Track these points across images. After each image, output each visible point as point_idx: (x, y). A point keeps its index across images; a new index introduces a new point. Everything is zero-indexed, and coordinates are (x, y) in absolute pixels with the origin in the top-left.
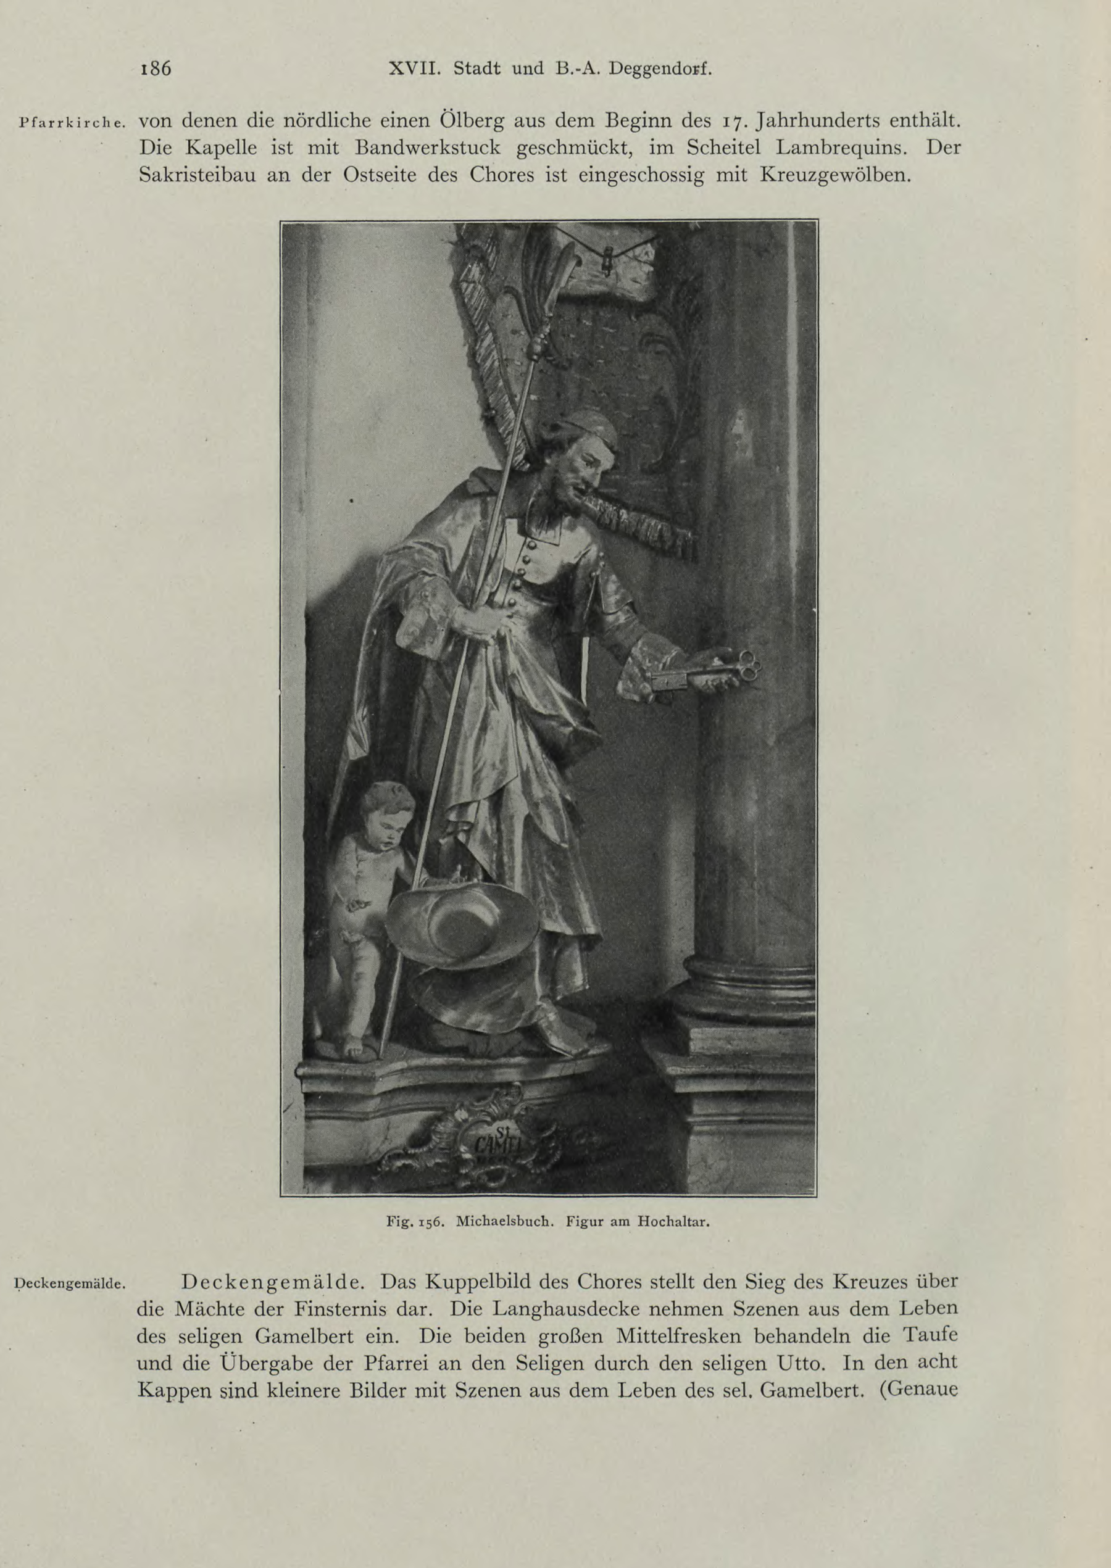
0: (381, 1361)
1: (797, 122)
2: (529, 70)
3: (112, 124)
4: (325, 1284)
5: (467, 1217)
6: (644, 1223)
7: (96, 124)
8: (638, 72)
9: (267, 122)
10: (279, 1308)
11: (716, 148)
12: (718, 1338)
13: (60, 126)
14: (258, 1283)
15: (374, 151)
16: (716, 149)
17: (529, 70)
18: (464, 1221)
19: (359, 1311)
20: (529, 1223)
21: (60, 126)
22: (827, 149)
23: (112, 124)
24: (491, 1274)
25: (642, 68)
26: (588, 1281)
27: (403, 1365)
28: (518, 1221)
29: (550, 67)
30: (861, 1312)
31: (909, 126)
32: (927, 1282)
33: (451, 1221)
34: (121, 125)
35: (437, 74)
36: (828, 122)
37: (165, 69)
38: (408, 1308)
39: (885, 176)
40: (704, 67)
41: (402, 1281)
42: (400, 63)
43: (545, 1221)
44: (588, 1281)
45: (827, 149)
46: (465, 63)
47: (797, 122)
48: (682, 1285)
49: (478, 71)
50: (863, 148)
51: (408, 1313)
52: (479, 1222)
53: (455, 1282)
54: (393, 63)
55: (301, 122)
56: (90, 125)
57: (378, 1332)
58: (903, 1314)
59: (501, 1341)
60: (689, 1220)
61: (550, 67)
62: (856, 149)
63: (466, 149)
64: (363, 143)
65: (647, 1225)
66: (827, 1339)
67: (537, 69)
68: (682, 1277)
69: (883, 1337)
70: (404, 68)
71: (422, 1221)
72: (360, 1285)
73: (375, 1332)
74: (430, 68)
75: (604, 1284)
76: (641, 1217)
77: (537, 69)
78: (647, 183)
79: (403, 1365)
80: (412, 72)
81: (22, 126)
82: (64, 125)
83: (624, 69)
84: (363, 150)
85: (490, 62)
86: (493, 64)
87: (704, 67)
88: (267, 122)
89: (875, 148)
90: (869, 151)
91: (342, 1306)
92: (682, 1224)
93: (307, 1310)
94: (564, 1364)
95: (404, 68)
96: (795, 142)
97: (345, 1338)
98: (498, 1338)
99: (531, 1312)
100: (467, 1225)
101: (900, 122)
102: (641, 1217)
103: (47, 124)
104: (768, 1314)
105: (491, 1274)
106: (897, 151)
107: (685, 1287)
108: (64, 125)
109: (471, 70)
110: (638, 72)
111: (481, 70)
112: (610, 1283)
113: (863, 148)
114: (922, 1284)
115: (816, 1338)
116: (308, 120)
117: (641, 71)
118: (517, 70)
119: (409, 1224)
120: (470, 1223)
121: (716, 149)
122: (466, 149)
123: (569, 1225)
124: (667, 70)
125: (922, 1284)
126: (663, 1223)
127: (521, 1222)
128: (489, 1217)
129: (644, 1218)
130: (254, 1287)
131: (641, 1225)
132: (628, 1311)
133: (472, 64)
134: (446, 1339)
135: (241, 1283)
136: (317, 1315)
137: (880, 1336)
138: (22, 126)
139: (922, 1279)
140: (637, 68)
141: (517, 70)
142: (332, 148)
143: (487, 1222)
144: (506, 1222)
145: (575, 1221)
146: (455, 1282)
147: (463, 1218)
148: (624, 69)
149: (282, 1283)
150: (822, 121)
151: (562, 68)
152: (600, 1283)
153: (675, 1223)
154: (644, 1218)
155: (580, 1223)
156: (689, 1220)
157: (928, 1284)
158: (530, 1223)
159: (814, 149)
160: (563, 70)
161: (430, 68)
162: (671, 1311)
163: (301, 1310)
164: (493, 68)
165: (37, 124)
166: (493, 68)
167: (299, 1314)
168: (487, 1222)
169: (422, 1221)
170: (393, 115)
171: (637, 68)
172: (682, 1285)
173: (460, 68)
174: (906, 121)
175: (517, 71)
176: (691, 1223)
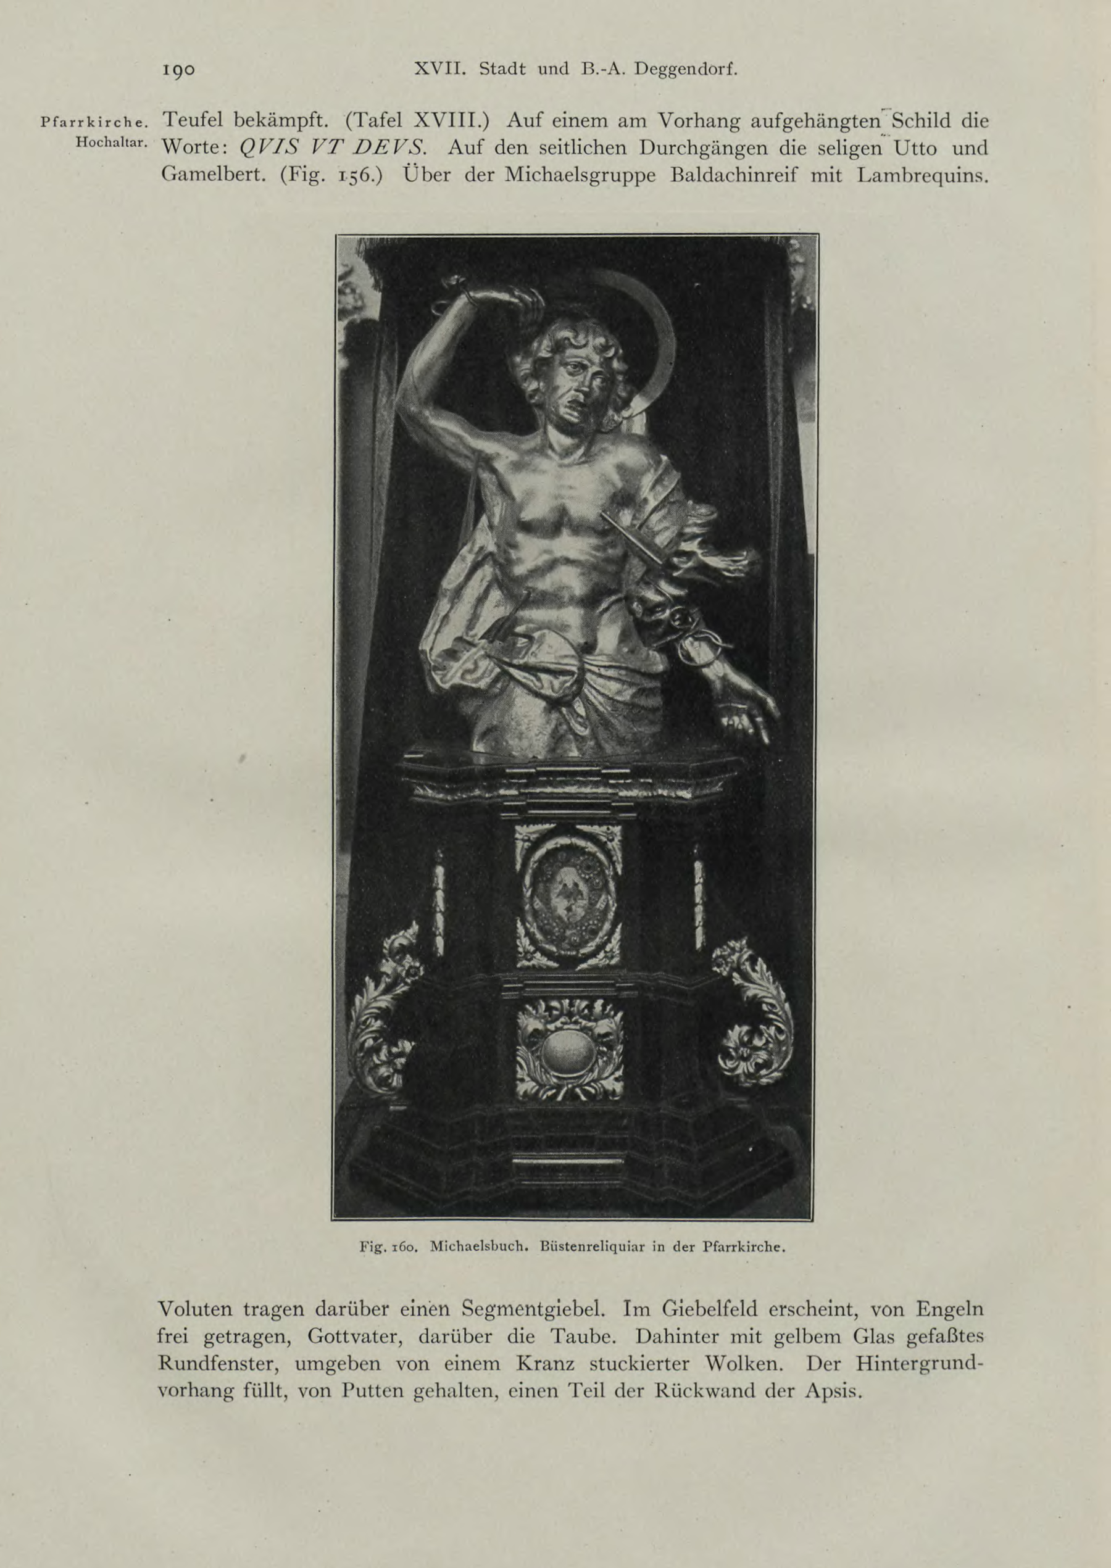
0: (55, 121)
1: (692, 123)
2: (555, 70)
3: (134, 124)
5: (441, 1243)
6: (82, 144)
7: (118, 124)
8: (668, 72)
10: (790, 1389)
13: (80, 126)
16: (599, 150)
17: (555, 70)
18: (438, 1246)
20: (503, 1248)
21: (80, 126)
22: (908, 177)
23: (134, 124)
25: (667, 69)
27: (731, 1249)
28: (492, 1246)
29: (576, 68)
33: (424, 1246)
35: (462, 75)
36: (970, 150)
37: (190, 70)
38: (430, 1335)
40: (729, 67)
41: (657, 1336)
42: (425, 63)
45: (908, 177)
46: (491, 64)
50: (944, 176)
51: (430, 1340)
52: (453, 1248)
53: (622, 175)
54: (418, 63)
56: (111, 124)
57: (456, 1359)
61: (576, 68)
62: (937, 177)
65: (85, 145)
67: (563, 70)
70: (429, 68)
73: (454, 1359)
74: (454, 68)
76: (79, 138)
77: (563, 70)
78: (593, 156)
79: (731, 1249)
80: (437, 72)
85: (515, 63)
86: (518, 65)
87: (729, 67)
89: (956, 176)
90: (950, 178)
91: (379, 1333)
94: (339, 1364)
96: (754, 116)
100: (441, 1250)
101: (869, 124)
102: (79, 138)
103: (68, 124)
106: (979, 179)
109: (496, 70)
110: (668, 72)
111: (506, 70)
113: (944, 176)
117: (667, 72)
118: (542, 70)
119: (382, 1249)
120: (444, 1248)
121: (599, 150)
123: (362, 1250)
124: (691, 70)
126: (574, 1248)
127: (495, 1247)
129: (82, 139)
131: (79, 145)
133: (129, 140)
140: (663, 69)
141: (542, 70)
142: (835, 176)
144: (480, 1248)
145: (369, 1248)
146: (622, 175)
147: (437, 1243)
151: (588, 68)
154: (82, 139)
155: (374, 1249)
158: (504, 1247)
159: (896, 177)
160: (589, 71)
161: (454, 68)
163: (295, 175)
164: (517, 69)
165: (58, 123)
166: (517, 69)
171: (663, 69)
173: (488, 68)
175: (543, 71)
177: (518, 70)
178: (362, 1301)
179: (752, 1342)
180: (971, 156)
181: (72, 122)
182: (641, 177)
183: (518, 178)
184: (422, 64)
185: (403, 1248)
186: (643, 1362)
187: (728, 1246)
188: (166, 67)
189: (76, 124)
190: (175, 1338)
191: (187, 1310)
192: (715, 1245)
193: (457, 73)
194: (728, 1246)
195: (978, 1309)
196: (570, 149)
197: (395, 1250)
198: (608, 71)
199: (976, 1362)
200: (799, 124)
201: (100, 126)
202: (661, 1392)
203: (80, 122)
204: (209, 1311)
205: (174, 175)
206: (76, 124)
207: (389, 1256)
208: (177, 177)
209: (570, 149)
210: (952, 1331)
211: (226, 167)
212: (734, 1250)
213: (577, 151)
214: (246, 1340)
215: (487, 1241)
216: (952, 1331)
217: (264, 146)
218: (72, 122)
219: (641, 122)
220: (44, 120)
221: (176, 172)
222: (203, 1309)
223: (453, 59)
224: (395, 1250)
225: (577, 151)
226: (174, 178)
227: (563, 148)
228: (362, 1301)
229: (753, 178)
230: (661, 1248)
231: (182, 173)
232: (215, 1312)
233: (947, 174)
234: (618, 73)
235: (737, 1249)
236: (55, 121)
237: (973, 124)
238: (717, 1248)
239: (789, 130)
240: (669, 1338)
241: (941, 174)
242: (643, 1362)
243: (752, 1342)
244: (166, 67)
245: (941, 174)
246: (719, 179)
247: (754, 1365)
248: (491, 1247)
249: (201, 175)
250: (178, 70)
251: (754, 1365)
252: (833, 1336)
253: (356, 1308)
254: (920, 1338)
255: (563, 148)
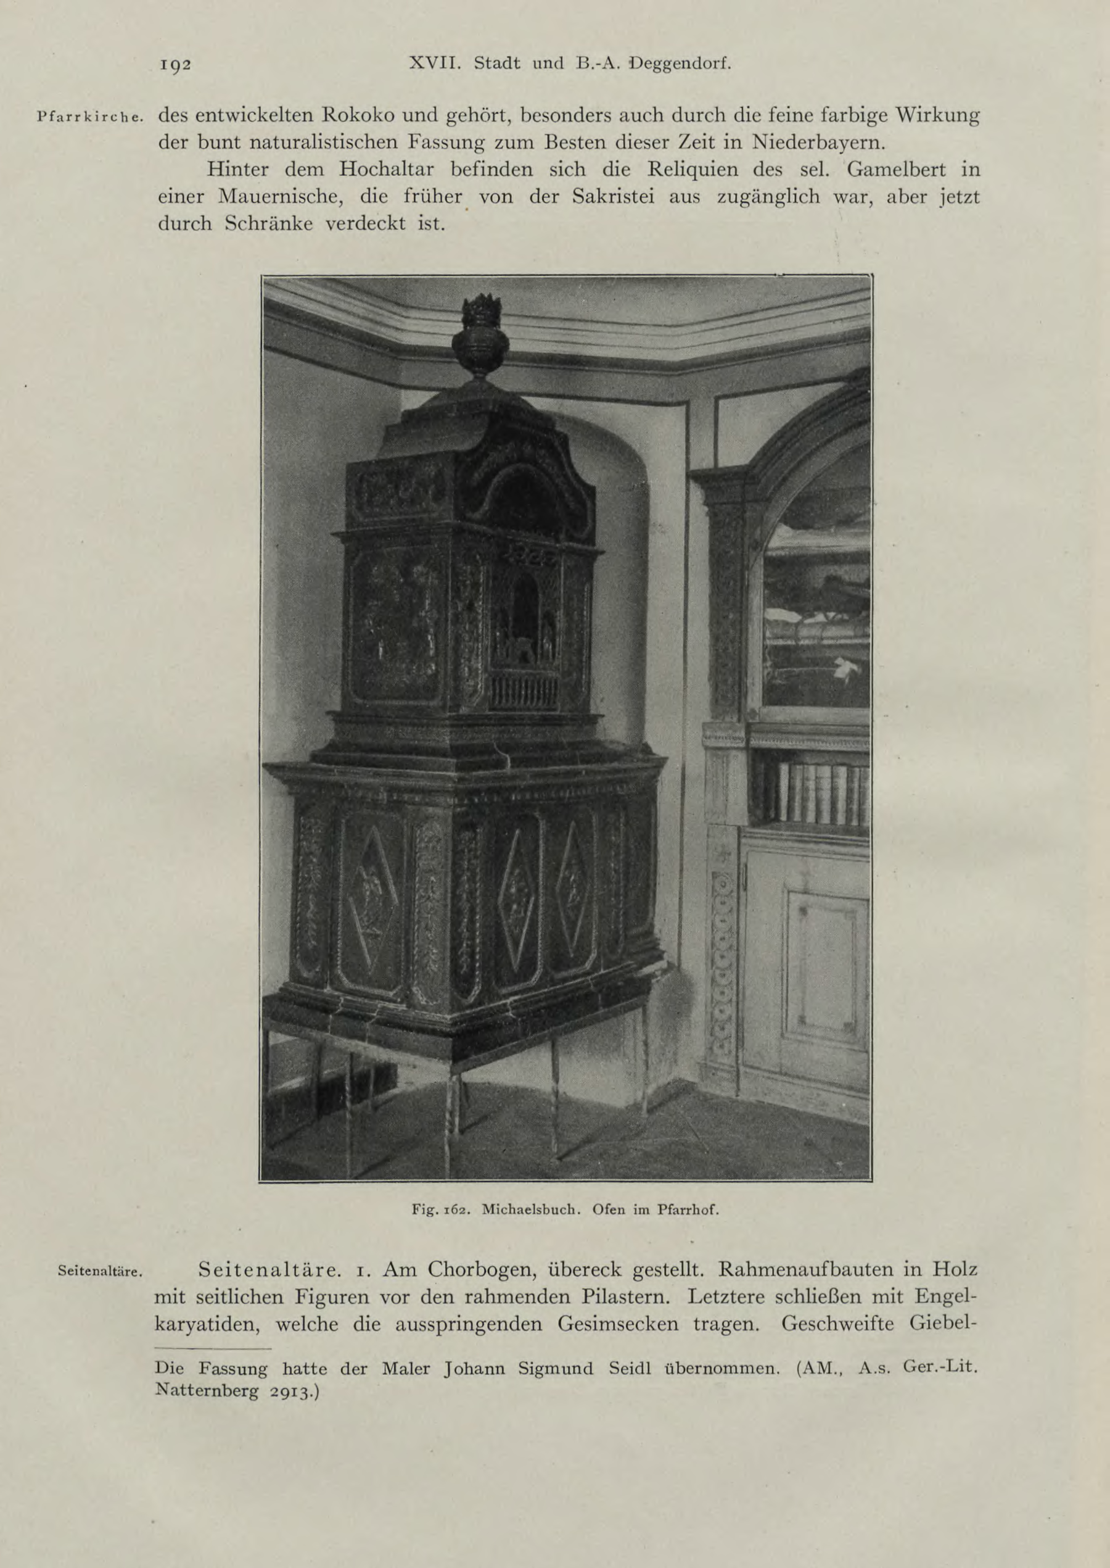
0: (52, 115)
1: (814, 144)
2: (549, 65)
3: (130, 119)
4: (283, 1271)
5: (492, 1206)
6: (348, 172)
7: (114, 118)
8: (662, 66)
9: (754, 117)
11: (370, 143)
12: (267, 117)
14: (262, 1271)
15: (832, 146)
18: (489, 1209)
19: (652, 1299)
20: (555, 1211)
23: (130, 119)
24: (682, 1262)
26: (438, 1269)
27: (685, 1212)
28: (544, 1210)
29: (571, 62)
30: (432, 1300)
31: (215, 120)
32: (942, 1268)
33: (477, 1208)
34: (139, 119)
39: (921, 171)
40: (723, 61)
42: (420, 57)
43: (571, 1210)
44: (438, 1269)
46: (486, 59)
47: (847, 117)
48: (686, 1272)
49: (499, 65)
50: (698, 170)
52: (504, 1211)
54: (413, 57)
55: (485, 117)
56: (108, 118)
58: (692, 1302)
59: (518, 1329)
60: (114, 1270)
63: (279, 143)
64: (552, 138)
66: (237, 1327)
68: (686, 1264)
69: (934, 1324)
70: (424, 62)
71: (447, 1209)
72: (336, 1273)
74: (449, 62)
75: (455, 1272)
79: (685, 1212)
81: (40, 120)
82: (82, 119)
83: (714, 64)
84: (552, 145)
85: (510, 57)
86: (513, 60)
87: (723, 61)
88: (754, 117)
92: (108, 1273)
93: (308, 1298)
95: (424, 62)
97: (719, 65)
98: (226, 1326)
99: (942, 1299)
104: (445, 1302)
105: (682, 1262)
107: (689, 1275)
108: (82, 119)
109: (491, 64)
110: (662, 66)
111: (501, 65)
112: (461, 1271)
113: (698, 170)
114: (554, 1272)
115: (514, 1326)
116: (492, 115)
117: (662, 66)
118: (537, 65)
119: (434, 1212)
120: (495, 1211)
122: (279, 143)
123: (415, 1213)
124: (686, 64)
125: (554, 1272)
127: (546, 1211)
128: (515, 1205)
130: (259, 1275)
132: (267, 117)
133: (492, 59)
134: (376, 1327)
135: (246, 1271)
136: (499, 1302)
137: (932, 1323)
138: (40, 120)
139: (553, 1266)
140: (657, 63)
141: (537, 65)
143: (512, 1211)
144: (532, 1211)
148: (714, 64)
149: (328, 1271)
150: (956, 115)
151: (583, 63)
152: (451, 1271)
153: (516, 1211)
154: (348, 165)
155: (426, 1211)
156: (114, 1270)
157: (560, 1272)
158: (555, 1211)
160: (584, 65)
161: (449, 62)
162: (468, 117)
163: (302, 1298)
164: (512, 63)
166: (512, 63)
167: (299, 1302)
168: (512, 1211)
169: (447, 1209)
170: (788, 110)
171: (657, 63)
172: (686, 1272)
173: (482, 63)
174: (212, 116)
176: (117, 1273)
177: (513, 64)
178: (563, 1262)
179: (175, 1302)
180: (180, 205)
181: (68, 116)
182: (504, 171)
183: (231, 199)
184: (417, 58)
185: (455, 1211)
186: (217, 1322)
187: (682, 1209)
188: (164, 62)
189: (73, 118)
190: (757, 1298)
191: (451, 1271)
192: (670, 1208)
193: (443, 67)
194: (682, 1209)
195: (916, 1270)
196: (227, 1298)
197: (447, 1213)
198: (603, 65)
199: (970, 1322)
200: (462, 118)
201: (973, 119)
202: (328, 116)
203: (77, 116)
204: (870, 1270)
205: (860, 171)
206: (73, 118)
207: (440, 1219)
208: (863, 173)
209: (227, 1298)
210: (834, 1291)
211: (912, 162)
212: (688, 1214)
213: (234, 1300)
214: (478, 1300)
215: (539, 1205)
216: (834, 1291)
217: (757, 141)
218: (68, 116)
219: (319, 170)
220: (41, 116)
221: (862, 167)
222: (865, 1270)
223: (448, 54)
224: (447, 1213)
225: (234, 1300)
226: (860, 174)
227: (220, 1297)
228: (563, 1262)
229: (231, 172)
230: (645, 1211)
231: (868, 169)
232: (639, 1300)
233: (701, 167)
234: (612, 67)
235: (691, 1212)
236: (52, 115)
237: (746, 118)
238: (672, 1211)
239: (873, 124)
240: (491, 1297)
241: (695, 168)
242: (217, 1322)
243: (893, 1302)
244: (164, 62)
245: (695, 168)
246: (395, 173)
247: (655, 1326)
248: (542, 1210)
249: (887, 170)
250: (176, 65)
251: (655, 1326)
252: (164, 1296)
253: (557, 1268)
254: (956, 1297)
255: (220, 1297)
